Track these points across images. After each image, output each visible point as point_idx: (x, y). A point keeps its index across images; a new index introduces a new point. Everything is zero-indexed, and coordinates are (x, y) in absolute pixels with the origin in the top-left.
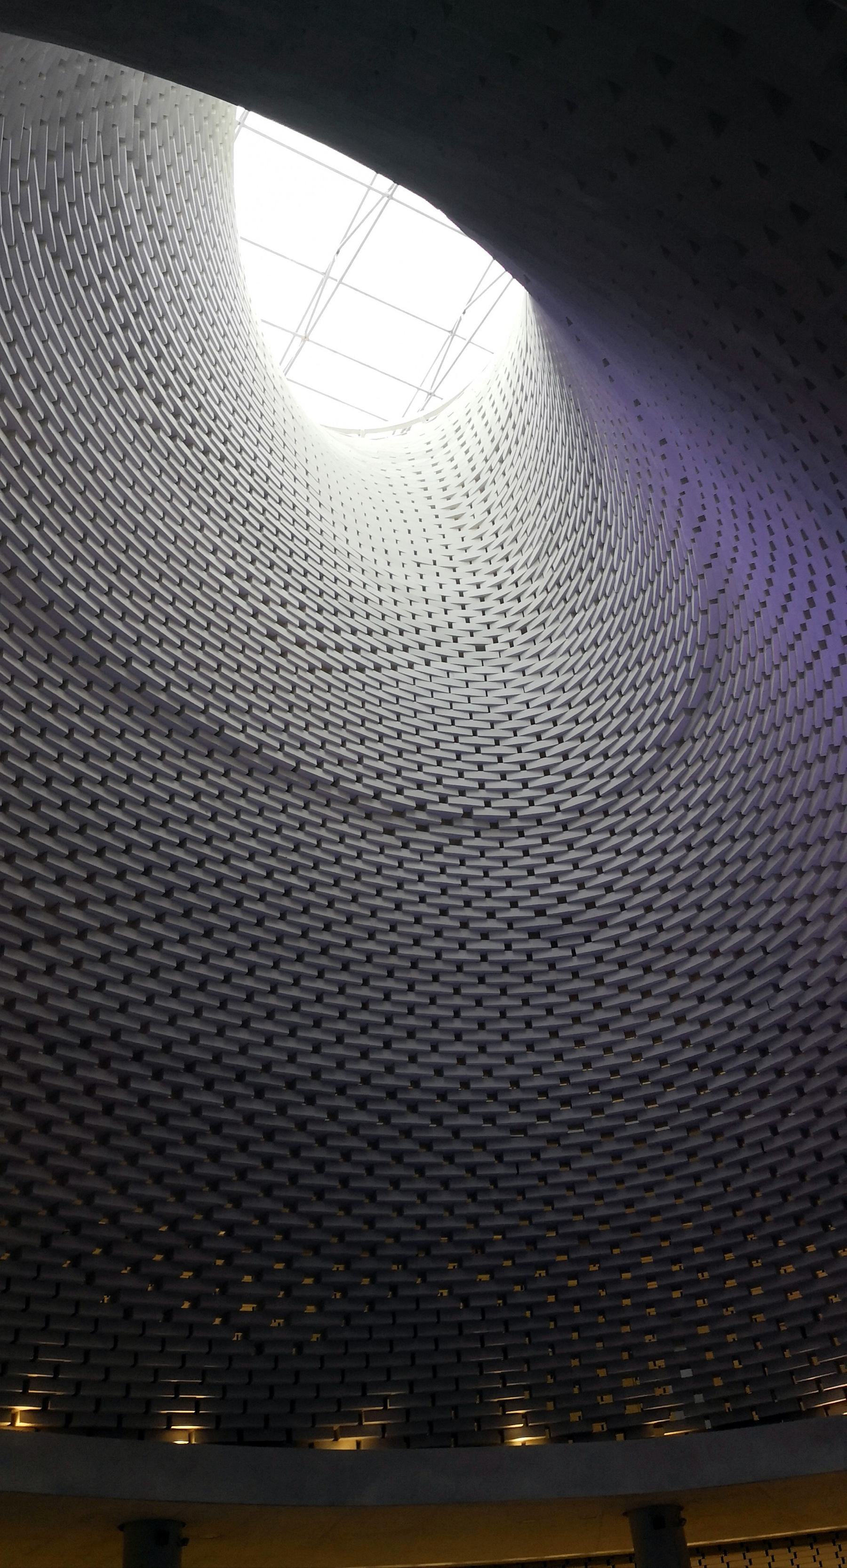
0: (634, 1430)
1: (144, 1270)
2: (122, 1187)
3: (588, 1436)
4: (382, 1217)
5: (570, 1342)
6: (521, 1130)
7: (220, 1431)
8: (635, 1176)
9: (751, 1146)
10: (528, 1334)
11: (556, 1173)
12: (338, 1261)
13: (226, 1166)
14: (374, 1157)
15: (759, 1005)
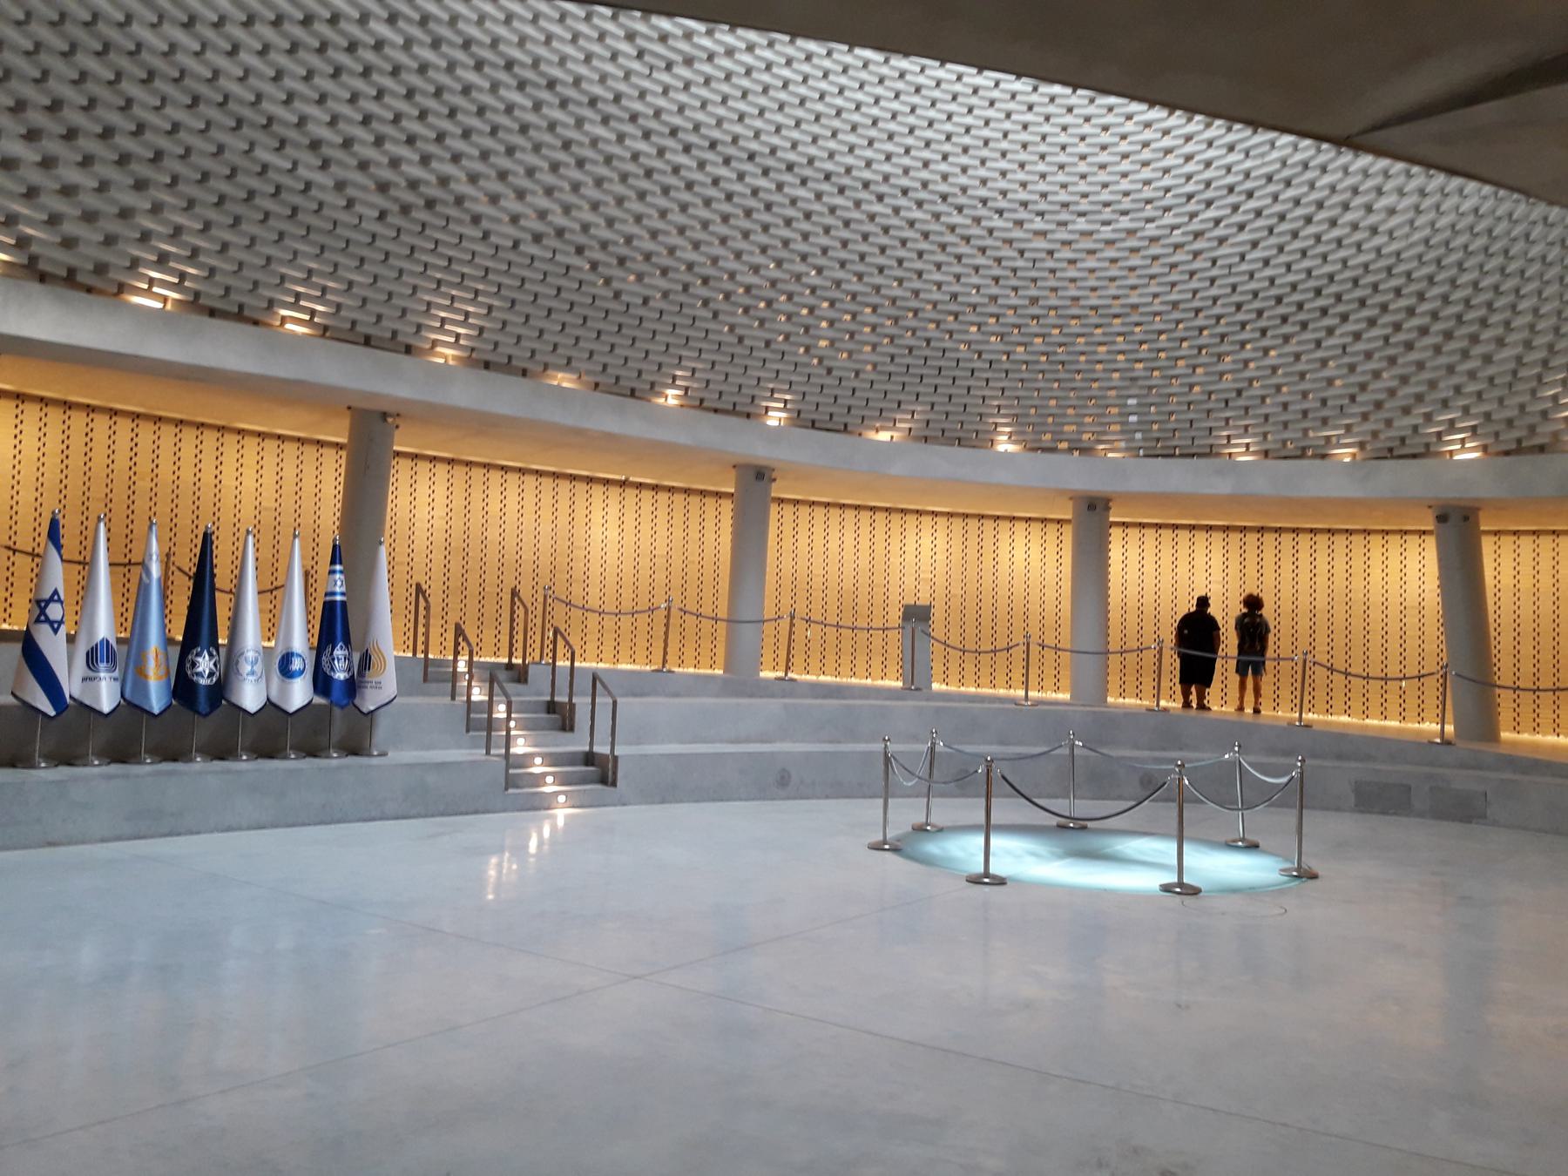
0: (1086, 451)
1: (752, 312)
2: (738, 255)
3: (1053, 450)
4: (925, 291)
5: (1052, 389)
6: (1044, 233)
7: (804, 420)
8: (1125, 277)
9: (1222, 267)
10: (1022, 380)
11: (1063, 270)
12: (889, 318)
13: (773, 236)
14: (924, 246)
15: (1255, 157)
